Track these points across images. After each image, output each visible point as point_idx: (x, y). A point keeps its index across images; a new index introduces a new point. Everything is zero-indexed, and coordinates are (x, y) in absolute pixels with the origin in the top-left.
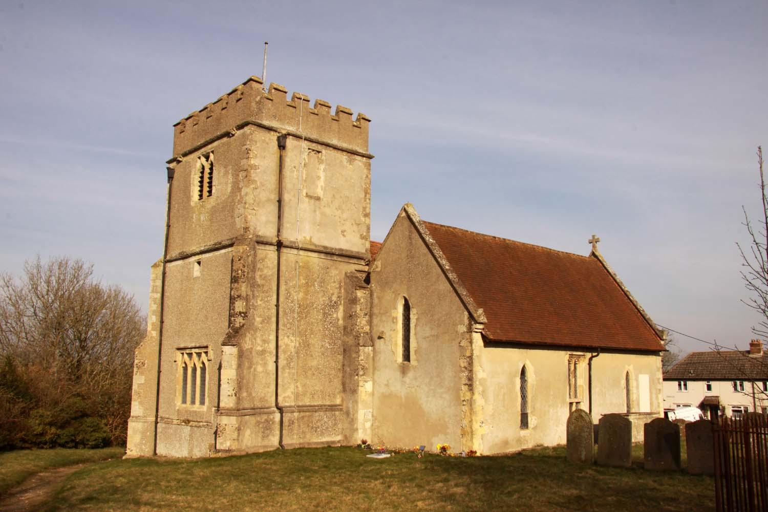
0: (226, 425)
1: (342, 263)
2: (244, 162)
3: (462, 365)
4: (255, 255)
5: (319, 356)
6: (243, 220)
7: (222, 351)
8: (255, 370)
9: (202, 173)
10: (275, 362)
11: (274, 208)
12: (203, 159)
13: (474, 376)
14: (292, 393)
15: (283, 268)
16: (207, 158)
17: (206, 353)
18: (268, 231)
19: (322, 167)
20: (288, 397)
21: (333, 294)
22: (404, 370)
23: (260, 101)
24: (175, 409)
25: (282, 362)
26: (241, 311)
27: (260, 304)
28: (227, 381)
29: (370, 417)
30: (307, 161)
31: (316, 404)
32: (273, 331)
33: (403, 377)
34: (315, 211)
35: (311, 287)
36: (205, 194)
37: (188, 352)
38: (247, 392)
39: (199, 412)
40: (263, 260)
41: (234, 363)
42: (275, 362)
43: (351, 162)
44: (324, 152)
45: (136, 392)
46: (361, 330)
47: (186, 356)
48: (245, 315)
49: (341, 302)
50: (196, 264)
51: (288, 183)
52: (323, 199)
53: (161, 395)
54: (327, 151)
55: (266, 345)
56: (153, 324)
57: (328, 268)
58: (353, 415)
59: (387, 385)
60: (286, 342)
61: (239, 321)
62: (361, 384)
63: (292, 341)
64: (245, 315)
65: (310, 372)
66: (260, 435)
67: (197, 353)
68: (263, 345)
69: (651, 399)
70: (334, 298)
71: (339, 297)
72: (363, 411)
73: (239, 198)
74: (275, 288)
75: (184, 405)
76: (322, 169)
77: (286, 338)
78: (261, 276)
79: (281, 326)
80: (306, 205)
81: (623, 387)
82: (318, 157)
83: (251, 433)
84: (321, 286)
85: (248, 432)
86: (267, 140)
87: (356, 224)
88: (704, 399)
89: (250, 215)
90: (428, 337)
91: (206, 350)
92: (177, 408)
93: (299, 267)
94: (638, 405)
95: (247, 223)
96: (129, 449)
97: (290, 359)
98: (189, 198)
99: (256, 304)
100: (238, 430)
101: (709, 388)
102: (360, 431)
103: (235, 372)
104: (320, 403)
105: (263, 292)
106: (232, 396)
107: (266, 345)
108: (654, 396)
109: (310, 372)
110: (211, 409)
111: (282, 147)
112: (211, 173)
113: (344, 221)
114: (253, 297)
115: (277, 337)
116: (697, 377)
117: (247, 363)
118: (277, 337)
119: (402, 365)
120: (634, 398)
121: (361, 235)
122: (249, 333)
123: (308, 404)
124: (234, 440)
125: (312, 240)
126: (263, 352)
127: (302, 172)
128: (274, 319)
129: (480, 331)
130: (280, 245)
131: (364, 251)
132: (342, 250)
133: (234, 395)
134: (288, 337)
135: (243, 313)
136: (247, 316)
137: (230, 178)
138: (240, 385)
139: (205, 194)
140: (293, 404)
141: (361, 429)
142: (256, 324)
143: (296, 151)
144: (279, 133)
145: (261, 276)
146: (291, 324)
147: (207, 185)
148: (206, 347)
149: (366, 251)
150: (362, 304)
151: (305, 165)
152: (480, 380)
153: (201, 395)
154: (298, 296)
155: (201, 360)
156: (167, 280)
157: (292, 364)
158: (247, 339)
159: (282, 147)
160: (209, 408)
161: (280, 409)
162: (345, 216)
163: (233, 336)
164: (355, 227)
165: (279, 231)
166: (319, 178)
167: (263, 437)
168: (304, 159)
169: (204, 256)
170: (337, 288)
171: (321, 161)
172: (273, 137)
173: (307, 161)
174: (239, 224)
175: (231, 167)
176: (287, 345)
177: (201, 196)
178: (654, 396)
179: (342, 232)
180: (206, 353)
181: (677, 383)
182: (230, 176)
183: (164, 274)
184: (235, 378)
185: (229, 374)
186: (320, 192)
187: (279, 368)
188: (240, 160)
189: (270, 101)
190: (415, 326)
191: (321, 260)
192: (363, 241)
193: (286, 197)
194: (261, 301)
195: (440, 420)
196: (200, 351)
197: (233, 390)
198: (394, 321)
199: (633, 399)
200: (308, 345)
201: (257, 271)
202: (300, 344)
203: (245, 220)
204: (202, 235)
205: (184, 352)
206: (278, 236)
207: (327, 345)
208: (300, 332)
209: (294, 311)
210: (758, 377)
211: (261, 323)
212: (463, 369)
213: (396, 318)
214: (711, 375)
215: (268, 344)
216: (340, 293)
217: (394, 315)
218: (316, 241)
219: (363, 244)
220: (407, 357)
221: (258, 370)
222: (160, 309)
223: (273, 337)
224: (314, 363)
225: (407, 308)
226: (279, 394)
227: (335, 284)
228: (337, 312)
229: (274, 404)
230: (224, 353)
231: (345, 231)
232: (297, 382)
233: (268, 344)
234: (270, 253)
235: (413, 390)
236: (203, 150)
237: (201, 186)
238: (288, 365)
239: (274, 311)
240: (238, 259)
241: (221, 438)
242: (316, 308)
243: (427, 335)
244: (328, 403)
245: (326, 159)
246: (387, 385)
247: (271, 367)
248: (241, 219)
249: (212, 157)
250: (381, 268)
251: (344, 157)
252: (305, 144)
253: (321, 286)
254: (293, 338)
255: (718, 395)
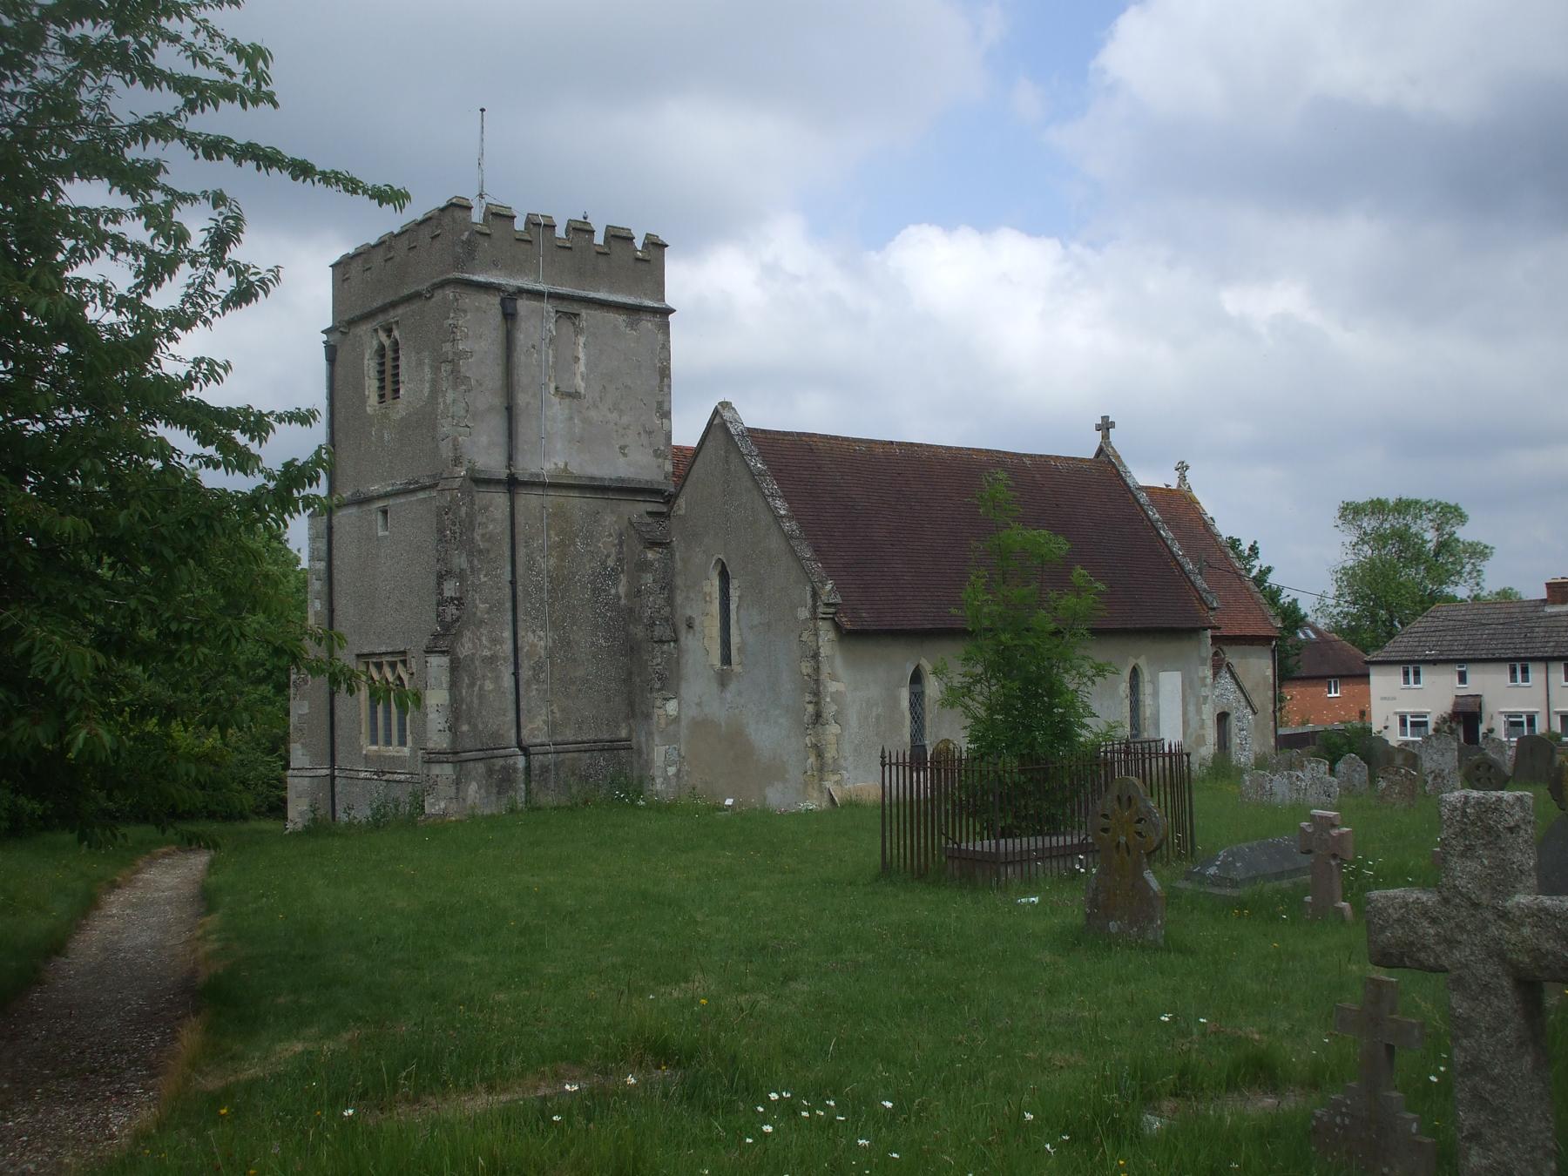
0: (437, 776)
1: (622, 502)
2: (447, 347)
3: (805, 671)
4: (472, 503)
5: (588, 660)
6: (451, 445)
7: (427, 662)
8: (481, 688)
9: (382, 356)
10: (513, 674)
11: (497, 422)
12: (383, 337)
13: (821, 688)
14: (544, 722)
15: (520, 519)
16: (389, 331)
17: (404, 662)
18: (491, 460)
19: (582, 340)
20: (538, 729)
21: (608, 556)
22: (723, 680)
23: (469, 241)
24: (361, 753)
25: (525, 673)
26: (453, 595)
27: (485, 582)
28: (436, 708)
29: (675, 757)
30: (554, 333)
31: (585, 739)
32: (508, 624)
33: (721, 692)
34: (571, 418)
35: (569, 546)
36: (388, 391)
37: (375, 660)
38: (469, 724)
39: (399, 757)
40: (486, 509)
41: (445, 679)
42: (513, 674)
43: (632, 325)
44: (584, 313)
45: (296, 728)
46: (657, 614)
47: (372, 667)
48: (459, 602)
49: (622, 569)
50: (379, 513)
51: (523, 376)
52: (585, 395)
53: (338, 732)
54: (589, 311)
55: (498, 647)
56: (316, 613)
57: (598, 513)
58: (648, 755)
59: (699, 705)
60: (530, 641)
61: (452, 610)
62: (658, 703)
63: (540, 638)
64: (459, 602)
65: (574, 688)
66: (495, 790)
67: (401, 661)
68: (493, 647)
69: (1185, 713)
70: (610, 563)
71: (619, 560)
72: (664, 748)
73: (442, 406)
74: (508, 553)
75: (375, 748)
76: (582, 344)
77: (529, 633)
78: (483, 535)
79: (521, 616)
80: (557, 409)
81: (1124, 696)
82: (574, 324)
83: (479, 788)
84: (588, 544)
85: (473, 786)
86: (484, 306)
87: (645, 431)
88: (1456, 704)
89: (460, 436)
90: (756, 626)
91: (402, 658)
92: (364, 752)
93: (548, 515)
94: (1157, 726)
95: (456, 449)
96: (291, 821)
97: (538, 668)
98: (363, 399)
99: (477, 582)
100: (457, 784)
101: (1462, 678)
102: (659, 781)
103: (448, 694)
104: (592, 737)
105: (489, 562)
106: (444, 731)
107: (498, 647)
108: (1192, 708)
109: (574, 688)
110: (416, 752)
111: (509, 316)
112: (396, 359)
113: (624, 429)
114: (471, 572)
115: (515, 634)
116: (1441, 657)
117: (466, 678)
118: (515, 634)
119: (720, 671)
120: (1148, 713)
121: (655, 451)
122: (469, 630)
123: (571, 739)
124: (451, 798)
125: (568, 468)
126: (491, 660)
127: (547, 355)
128: (508, 605)
129: (831, 616)
130: (512, 484)
131: (661, 478)
132: (623, 480)
133: (446, 729)
134: (534, 632)
135: (456, 599)
136: (463, 604)
137: (427, 373)
138: (456, 712)
139: (388, 391)
140: (545, 740)
141: (660, 777)
142: (479, 614)
143: (536, 323)
144: (503, 291)
145: (483, 535)
146: (538, 610)
147: (389, 385)
148: (404, 653)
149: (666, 478)
150: (656, 571)
151: (551, 340)
152: (832, 694)
153: (399, 730)
154: (547, 563)
155: (396, 675)
156: (336, 537)
157: (542, 676)
158: (465, 640)
159: (509, 316)
160: (413, 751)
161: (525, 750)
162: (625, 420)
163: (444, 638)
164: (644, 439)
165: (510, 458)
166: (577, 359)
167: (499, 793)
168: (550, 331)
169: (391, 502)
170: (615, 545)
171: (578, 331)
172: (495, 300)
173: (554, 333)
174: (446, 451)
175: (427, 353)
176: (533, 645)
177: (382, 396)
178: (1192, 708)
179: (620, 448)
180: (404, 662)
181: (1400, 670)
182: (427, 369)
183: (330, 528)
184: (447, 702)
185: (437, 697)
186: (581, 385)
187: (521, 683)
188: (298, 643)
189: (486, 237)
190: (737, 607)
191: (585, 500)
192: (660, 460)
193: (522, 399)
194: (485, 576)
195: (774, 759)
196: (394, 659)
197: (446, 722)
198: (706, 599)
199: (1144, 715)
200: (568, 643)
201: (477, 527)
202: (554, 642)
203: (454, 445)
204: (387, 465)
205: (370, 660)
206: (509, 466)
207: (601, 641)
208: (553, 622)
209: (542, 588)
210: (1556, 654)
211: (488, 613)
212: (806, 677)
213: (710, 595)
214: (1466, 652)
215: (501, 645)
216: (620, 553)
217: (707, 589)
218: (575, 468)
219: (659, 467)
220: (726, 659)
221: (486, 688)
222: (326, 589)
223: (507, 634)
224: (580, 673)
225: (725, 577)
226: (522, 725)
227: (611, 538)
228: (616, 585)
229: (514, 742)
230: (428, 665)
231: (626, 447)
232: (551, 705)
233: (501, 645)
234: (500, 499)
235: (737, 711)
236: (381, 318)
237: (382, 380)
238: (536, 678)
239: (508, 591)
240: (443, 513)
241: (431, 796)
242: (579, 580)
243: (755, 623)
244: (606, 737)
245: (587, 326)
246: (699, 705)
247: (508, 681)
248: (448, 443)
249: (396, 333)
250: (686, 508)
251: (620, 319)
252: (548, 307)
253: (588, 544)
254: (542, 633)
255: (1480, 693)
